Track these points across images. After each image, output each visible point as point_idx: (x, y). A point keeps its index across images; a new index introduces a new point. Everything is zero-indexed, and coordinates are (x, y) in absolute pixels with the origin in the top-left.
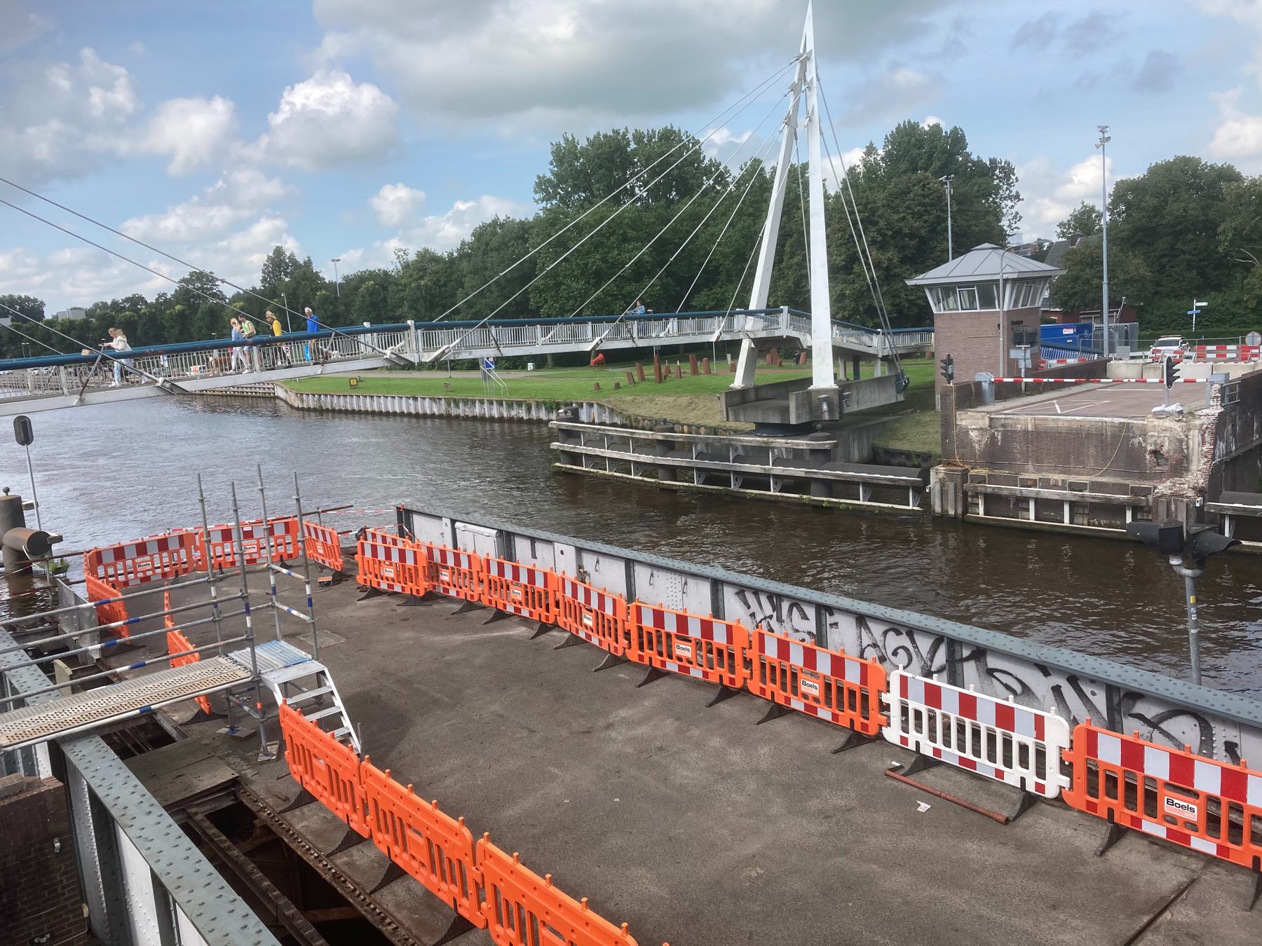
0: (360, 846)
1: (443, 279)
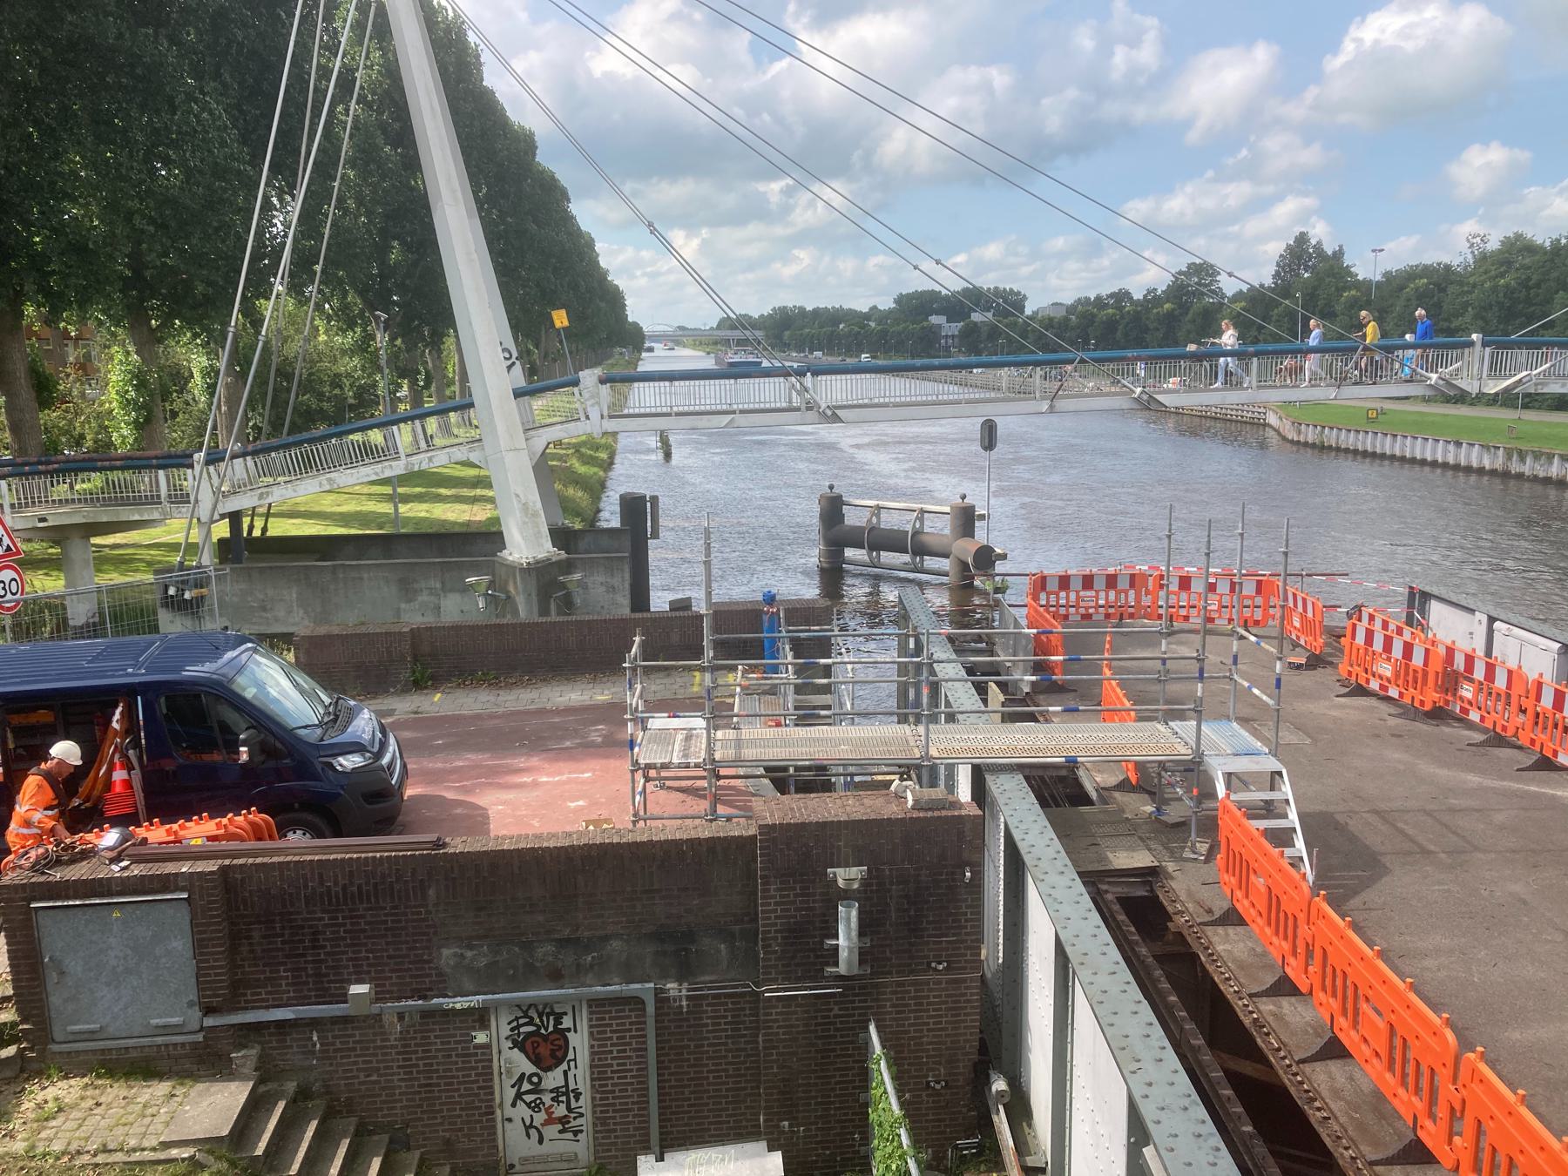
0: (1293, 999)
1: (1535, 278)
